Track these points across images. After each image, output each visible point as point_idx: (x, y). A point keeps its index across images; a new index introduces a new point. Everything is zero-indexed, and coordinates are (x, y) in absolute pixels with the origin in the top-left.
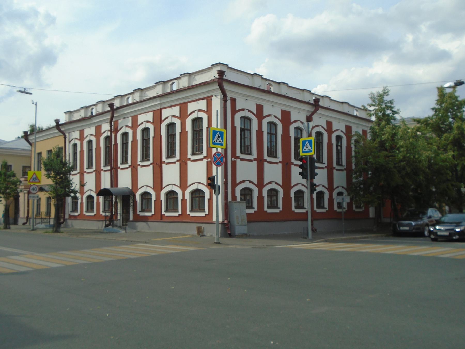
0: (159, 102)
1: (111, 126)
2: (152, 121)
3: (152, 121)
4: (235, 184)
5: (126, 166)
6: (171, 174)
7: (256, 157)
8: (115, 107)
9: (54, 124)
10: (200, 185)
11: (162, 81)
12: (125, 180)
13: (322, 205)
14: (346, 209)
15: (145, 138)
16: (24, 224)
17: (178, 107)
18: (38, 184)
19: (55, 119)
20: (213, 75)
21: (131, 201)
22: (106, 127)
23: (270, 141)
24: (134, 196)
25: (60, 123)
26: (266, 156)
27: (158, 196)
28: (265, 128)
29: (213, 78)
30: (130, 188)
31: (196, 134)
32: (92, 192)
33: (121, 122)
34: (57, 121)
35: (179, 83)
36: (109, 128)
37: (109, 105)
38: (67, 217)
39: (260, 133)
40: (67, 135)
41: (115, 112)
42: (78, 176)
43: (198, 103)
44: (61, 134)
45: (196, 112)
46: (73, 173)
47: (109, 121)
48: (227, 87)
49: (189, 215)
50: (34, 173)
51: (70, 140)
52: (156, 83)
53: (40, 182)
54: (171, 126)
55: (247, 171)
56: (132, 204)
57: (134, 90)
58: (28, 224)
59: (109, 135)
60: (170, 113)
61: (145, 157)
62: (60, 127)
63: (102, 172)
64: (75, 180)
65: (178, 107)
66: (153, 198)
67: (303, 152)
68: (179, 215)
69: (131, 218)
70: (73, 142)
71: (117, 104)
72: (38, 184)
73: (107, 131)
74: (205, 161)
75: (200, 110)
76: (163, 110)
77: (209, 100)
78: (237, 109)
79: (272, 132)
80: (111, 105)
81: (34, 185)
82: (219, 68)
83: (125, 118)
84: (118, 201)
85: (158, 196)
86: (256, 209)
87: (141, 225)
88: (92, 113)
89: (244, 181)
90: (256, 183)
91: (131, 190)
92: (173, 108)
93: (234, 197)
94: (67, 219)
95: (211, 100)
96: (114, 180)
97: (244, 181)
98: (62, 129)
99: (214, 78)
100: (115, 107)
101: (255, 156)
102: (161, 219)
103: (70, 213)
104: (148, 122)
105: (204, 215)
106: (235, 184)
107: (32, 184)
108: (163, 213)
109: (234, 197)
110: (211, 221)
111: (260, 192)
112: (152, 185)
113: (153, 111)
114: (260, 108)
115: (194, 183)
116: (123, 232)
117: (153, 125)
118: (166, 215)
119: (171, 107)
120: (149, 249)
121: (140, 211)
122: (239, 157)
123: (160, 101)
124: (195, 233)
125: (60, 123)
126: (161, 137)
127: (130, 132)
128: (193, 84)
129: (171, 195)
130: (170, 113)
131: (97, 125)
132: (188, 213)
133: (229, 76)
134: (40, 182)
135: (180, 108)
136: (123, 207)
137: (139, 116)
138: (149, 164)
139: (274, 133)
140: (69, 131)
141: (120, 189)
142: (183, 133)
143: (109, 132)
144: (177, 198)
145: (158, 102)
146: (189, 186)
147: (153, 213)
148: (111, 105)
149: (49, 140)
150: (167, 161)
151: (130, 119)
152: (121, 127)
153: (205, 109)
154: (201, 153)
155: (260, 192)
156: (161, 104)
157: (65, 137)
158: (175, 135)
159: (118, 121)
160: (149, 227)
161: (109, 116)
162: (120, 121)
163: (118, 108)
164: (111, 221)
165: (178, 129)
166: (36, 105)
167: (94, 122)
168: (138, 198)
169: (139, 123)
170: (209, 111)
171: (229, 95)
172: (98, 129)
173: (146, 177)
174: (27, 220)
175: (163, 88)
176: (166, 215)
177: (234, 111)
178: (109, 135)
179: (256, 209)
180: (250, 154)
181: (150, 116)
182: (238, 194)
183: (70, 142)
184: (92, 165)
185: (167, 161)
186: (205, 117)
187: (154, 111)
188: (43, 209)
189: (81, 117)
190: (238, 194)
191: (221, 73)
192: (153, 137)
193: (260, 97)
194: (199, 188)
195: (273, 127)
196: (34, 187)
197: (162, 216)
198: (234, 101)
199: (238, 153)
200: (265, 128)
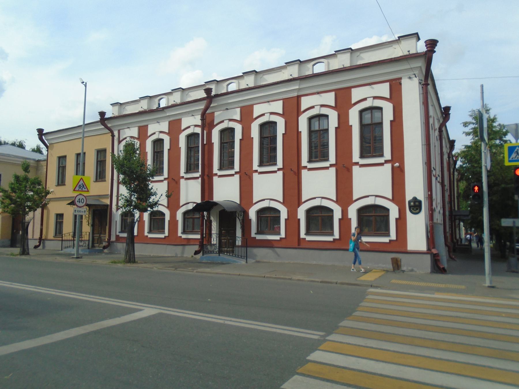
0: (297, 87)
7: (281, 167)
9: (98, 118)
10: (323, 200)
11: (181, 88)
12: (226, 190)
13: (366, 230)
15: (99, 159)
16: (36, 247)
17: (387, 84)
18: (85, 194)
19: (99, 111)
24: (246, 214)
25: (106, 116)
26: (356, 157)
27: (173, 216)
30: (238, 202)
31: (157, 156)
33: (218, 115)
34: (102, 114)
35: (328, 63)
38: (113, 239)
40: (116, 133)
41: (213, 100)
43: (195, 118)
44: (107, 131)
45: (192, 127)
46: (156, 178)
49: (147, 236)
50: (82, 179)
51: (121, 139)
52: (286, 63)
53: (88, 191)
54: (268, 128)
58: (41, 247)
60: (313, 103)
62: (106, 122)
63: (182, 181)
64: (159, 188)
65: (281, 102)
66: (167, 218)
67: (510, 161)
68: (165, 237)
69: (239, 242)
72: (85, 194)
74: (389, 166)
76: (303, 99)
80: (208, 91)
81: (81, 194)
83: (227, 109)
84: (212, 218)
85: (173, 216)
87: (260, 253)
88: (159, 104)
91: (240, 205)
92: (323, 95)
94: (113, 242)
95: (401, 84)
98: (109, 125)
99: (408, 53)
102: (299, 244)
103: (118, 234)
105: (279, 239)
107: (78, 193)
108: (303, 235)
110: (403, 250)
113: (283, 99)
115: (264, 200)
116: (243, 262)
117: (169, 136)
118: (307, 239)
119: (318, 93)
121: (119, 232)
122: (306, 167)
123: (299, 85)
124: (390, 267)
125: (106, 116)
126: (299, 134)
128: (307, 74)
131: (171, 119)
132: (146, 234)
134: (88, 191)
135: (283, 102)
136: (225, 228)
137: (353, 90)
140: (119, 128)
144: (164, 219)
145: (295, 86)
146: (182, 206)
147: (167, 234)
148: (208, 91)
149: (90, 137)
150: (310, 166)
151: (238, 110)
152: (124, 137)
154: (275, 164)
156: (299, 90)
157: (113, 136)
158: (162, 152)
159: (213, 113)
160: (278, 255)
161: (202, 106)
162: (216, 114)
163: (217, 96)
164: (203, 246)
166: (86, 86)
167: (168, 115)
170: (395, 96)
173: (268, 188)
174: (40, 242)
175: (149, 104)
176: (307, 239)
181: (164, 126)
183: (120, 142)
185: (310, 166)
186: (238, 129)
187: (285, 101)
188: (68, 228)
192: (169, 150)
194: (271, 206)
196: (81, 197)
197: (300, 241)
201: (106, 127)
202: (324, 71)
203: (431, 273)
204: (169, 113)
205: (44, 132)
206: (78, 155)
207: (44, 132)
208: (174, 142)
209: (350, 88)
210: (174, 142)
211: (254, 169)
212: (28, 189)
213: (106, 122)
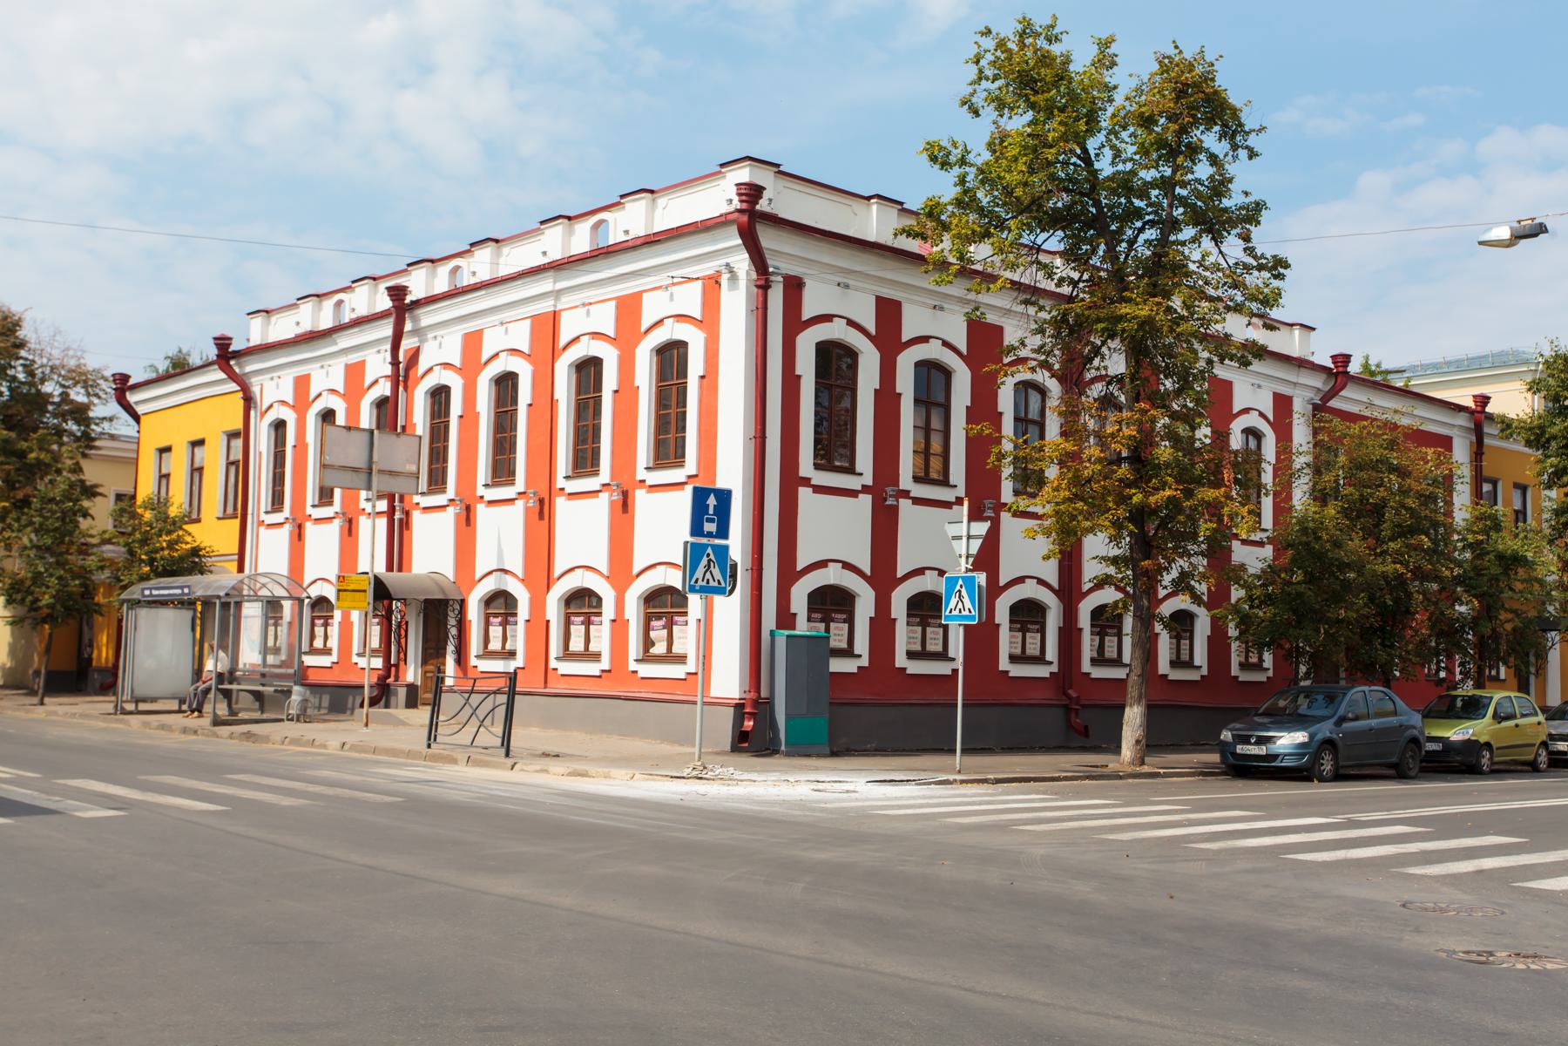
1: (395, 363)
2: (458, 364)
3: (458, 364)
4: (789, 574)
5: (440, 500)
6: (582, 531)
8: (408, 300)
9: (212, 353)
12: (432, 552)
14: (1054, 668)
19: (217, 334)
20: (720, 198)
21: (452, 621)
22: (378, 366)
23: (925, 429)
28: (905, 383)
29: (724, 208)
30: (452, 578)
32: (508, 577)
36: (388, 370)
37: (389, 289)
39: (887, 399)
42: (449, 517)
44: (233, 386)
47: (388, 346)
48: (768, 239)
55: (834, 530)
56: (454, 631)
57: (472, 245)
59: (388, 393)
61: (502, 471)
62: (232, 362)
70: (271, 417)
71: (418, 284)
73: (382, 381)
75: (681, 317)
77: (712, 284)
78: (806, 316)
79: (933, 399)
80: (397, 293)
82: (743, 174)
86: (865, 662)
89: (822, 564)
90: (868, 572)
93: (785, 618)
96: (398, 553)
97: (822, 564)
100: (408, 300)
101: (868, 479)
104: (596, 335)
106: (789, 574)
108: (553, 664)
109: (785, 618)
111: (883, 604)
112: (604, 567)
114: (889, 311)
120: (339, 791)
126: (553, 403)
127: (610, 357)
129: (582, 602)
130: (587, 319)
133: (781, 200)
135: (617, 307)
137: (486, 333)
138: (445, 503)
139: (942, 400)
141: (417, 576)
142: (626, 391)
143: (389, 384)
145: (546, 284)
146: (638, 575)
148: (397, 293)
153: (697, 315)
155: (883, 604)
158: (598, 402)
161: (386, 329)
163: (417, 304)
165: (695, 367)
168: (474, 613)
169: (486, 354)
170: (709, 321)
171: (780, 265)
172: (355, 373)
177: (794, 324)
178: (388, 393)
179: (865, 662)
180: (850, 470)
181: (521, 336)
182: (799, 604)
184: (512, 473)
189: (299, 331)
190: (799, 604)
191: (752, 193)
193: (889, 275)
195: (937, 377)
198: (794, 287)
199: (806, 467)
200: (905, 383)
201: (233, 376)
202: (587, 249)
203: (115, 694)
204: (345, 341)
205: (131, 382)
206: (232, 435)
207: (131, 382)
208: (545, 381)
209: (640, 294)
210: (545, 381)
211: (639, 477)
212: (1182, 430)
213: (232, 362)
